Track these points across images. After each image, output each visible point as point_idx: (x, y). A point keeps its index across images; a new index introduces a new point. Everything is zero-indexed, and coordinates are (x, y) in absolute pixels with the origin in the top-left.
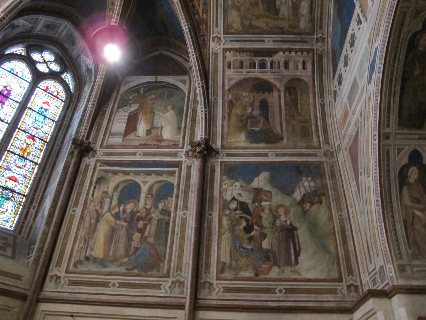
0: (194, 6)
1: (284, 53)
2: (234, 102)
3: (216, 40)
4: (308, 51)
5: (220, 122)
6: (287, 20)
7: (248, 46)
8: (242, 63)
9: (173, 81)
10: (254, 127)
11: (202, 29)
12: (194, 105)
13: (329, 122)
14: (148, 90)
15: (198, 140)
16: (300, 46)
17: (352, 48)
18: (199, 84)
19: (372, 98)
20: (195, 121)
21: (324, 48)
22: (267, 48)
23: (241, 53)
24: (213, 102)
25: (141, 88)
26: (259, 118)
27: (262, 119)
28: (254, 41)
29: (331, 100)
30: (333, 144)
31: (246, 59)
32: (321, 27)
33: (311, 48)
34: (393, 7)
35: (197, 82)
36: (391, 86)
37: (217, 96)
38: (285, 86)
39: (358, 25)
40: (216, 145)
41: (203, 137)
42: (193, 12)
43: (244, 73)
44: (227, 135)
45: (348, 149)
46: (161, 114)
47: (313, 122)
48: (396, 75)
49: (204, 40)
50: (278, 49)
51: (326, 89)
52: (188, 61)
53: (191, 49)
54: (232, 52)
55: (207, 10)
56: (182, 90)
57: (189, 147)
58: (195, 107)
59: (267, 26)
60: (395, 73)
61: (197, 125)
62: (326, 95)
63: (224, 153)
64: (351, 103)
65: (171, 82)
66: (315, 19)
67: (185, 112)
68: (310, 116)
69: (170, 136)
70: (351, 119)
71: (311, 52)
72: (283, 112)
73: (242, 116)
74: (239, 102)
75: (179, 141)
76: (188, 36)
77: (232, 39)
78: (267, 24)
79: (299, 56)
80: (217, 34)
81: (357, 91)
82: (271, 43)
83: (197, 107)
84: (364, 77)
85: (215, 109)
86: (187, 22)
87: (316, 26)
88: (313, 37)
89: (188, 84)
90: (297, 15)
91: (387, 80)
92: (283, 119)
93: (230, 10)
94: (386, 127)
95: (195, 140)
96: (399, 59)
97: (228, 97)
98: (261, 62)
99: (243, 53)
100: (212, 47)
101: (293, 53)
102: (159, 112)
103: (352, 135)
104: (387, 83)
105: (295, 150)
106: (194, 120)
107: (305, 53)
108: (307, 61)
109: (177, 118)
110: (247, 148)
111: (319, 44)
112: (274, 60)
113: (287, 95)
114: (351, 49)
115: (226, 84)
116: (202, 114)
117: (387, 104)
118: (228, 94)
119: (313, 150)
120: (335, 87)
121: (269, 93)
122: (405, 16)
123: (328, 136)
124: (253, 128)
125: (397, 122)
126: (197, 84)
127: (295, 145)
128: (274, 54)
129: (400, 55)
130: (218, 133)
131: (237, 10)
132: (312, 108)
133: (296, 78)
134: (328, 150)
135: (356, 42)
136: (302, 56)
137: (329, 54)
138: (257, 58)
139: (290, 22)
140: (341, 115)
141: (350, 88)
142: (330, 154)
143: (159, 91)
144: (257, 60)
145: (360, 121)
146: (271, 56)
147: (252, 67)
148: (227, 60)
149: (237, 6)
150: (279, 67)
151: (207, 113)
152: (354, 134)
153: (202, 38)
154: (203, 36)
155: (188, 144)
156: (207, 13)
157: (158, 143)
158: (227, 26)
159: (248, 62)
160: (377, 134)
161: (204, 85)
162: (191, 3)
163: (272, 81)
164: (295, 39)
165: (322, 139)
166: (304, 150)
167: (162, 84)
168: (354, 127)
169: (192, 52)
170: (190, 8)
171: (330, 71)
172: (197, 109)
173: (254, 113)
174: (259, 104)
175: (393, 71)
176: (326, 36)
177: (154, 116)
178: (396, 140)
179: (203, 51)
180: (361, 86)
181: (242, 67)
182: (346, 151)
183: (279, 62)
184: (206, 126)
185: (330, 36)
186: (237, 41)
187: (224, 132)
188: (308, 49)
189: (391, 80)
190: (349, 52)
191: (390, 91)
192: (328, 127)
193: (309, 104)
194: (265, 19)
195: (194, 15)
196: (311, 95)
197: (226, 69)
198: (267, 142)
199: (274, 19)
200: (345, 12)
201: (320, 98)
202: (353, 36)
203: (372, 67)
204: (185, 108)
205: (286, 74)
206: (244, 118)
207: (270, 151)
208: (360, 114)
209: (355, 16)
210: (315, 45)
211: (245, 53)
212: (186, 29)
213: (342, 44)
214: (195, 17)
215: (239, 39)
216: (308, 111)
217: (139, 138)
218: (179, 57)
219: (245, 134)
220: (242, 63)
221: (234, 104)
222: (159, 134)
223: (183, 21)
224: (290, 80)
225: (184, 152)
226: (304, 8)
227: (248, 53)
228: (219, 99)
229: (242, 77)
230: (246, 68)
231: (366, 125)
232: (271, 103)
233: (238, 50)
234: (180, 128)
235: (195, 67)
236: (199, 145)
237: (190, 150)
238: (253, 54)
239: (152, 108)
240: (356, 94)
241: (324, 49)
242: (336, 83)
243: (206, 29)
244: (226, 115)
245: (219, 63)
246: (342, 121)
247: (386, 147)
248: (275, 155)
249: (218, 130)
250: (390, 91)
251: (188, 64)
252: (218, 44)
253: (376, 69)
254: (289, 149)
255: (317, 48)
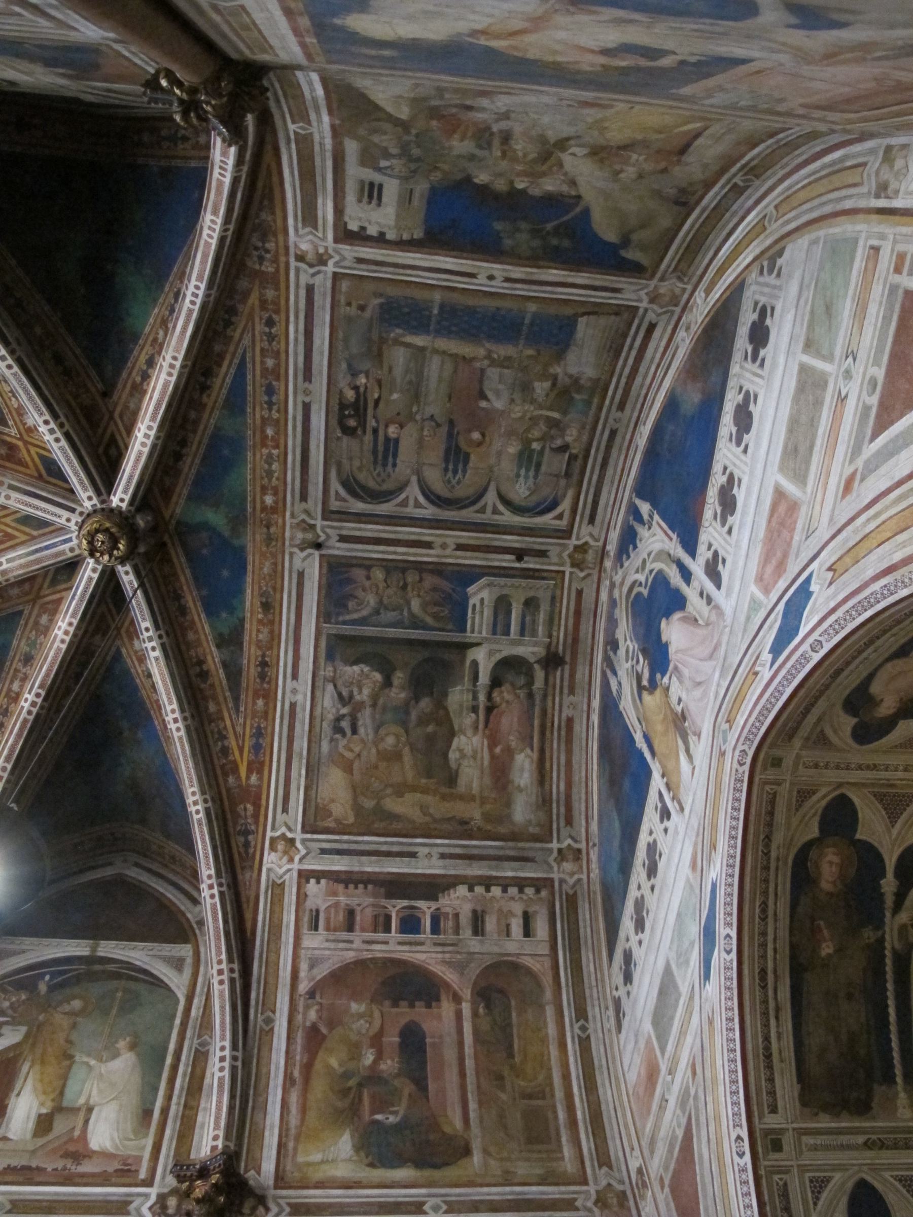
0: (225, 751)
1: (471, 889)
2: (324, 1030)
3: (281, 846)
4: (539, 884)
5: (276, 1095)
6: (478, 801)
7: (370, 866)
8: (351, 913)
9: (146, 959)
10: (378, 1113)
11: (243, 813)
12: (199, 1036)
13: (606, 1093)
14: (61, 985)
15: (203, 1154)
16: (513, 870)
17: (652, 880)
18: (220, 972)
19: (717, 1024)
20: (200, 1089)
21: (581, 876)
22: (424, 875)
23: (351, 886)
24: (262, 1030)
25: (42, 976)
26: (396, 1083)
27: (408, 1088)
28: (388, 854)
29: (606, 1026)
30: (623, 1168)
31: (365, 904)
32: (569, 821)
33: (545, 876)
34: (742, 781)
35: (216, 967)
36: (764, 987)
37: (274, 1012)
38: (475, 983)
39: (662, 821)
40: (259, 1173)
41: (220, 1146)
42: (222, 767)
43: (357, 944)
44: (297, 1139)
45: (667, 1182)
46: (93, 1062)
47: (559, 1094)
48: (775, 959)
49: (247, 844)
50: (456, 876)
51: (592, 993)
52: (195, 902)
53: (207, 870)
54: (323, 881)
55: (262, 764)
56: (169, 989)
57: (171, 1181)
58: (203, 1044)
59: (425, 815)
60: (770, 953)
61: (202, 1105)
62: (593, 1011)
63: (282, 1202)
64: (662, 1037)
65: (138, 963)
66: (551, 799)
67: (169, 1060)
68: (550, 1077)
69: (112, 1139)
70: (668, 1087)
71: (545, 886)
72: (469, 1063)
73: (346, 1076)
74: (339, 1031)
75: (139, 1159)
76: (201, 832)
77: (325, 845)
78: (424, 809)
79: (512, 898)
80: (284, 829)
81: (677, 1001)
82: (435, 861)
83: (209, 1044)
84: (692, 963)
85: (264, 1053)
86: (203, 793)
87: (555, 817)
88: (549, 846)
89: (188, 971)
90: (504, 787)
91: (752, 971)
92: (469, 1088)
93: (323, 768)
94: (766, 1111)
95: (192, 1156)
96: (775, 914)
97: (305, 1014)
98: (408, 912)
99: (356, 888)
100: (270, 866)
101: (496, 891)
102: (89, 1055)
103: (674, 1137)
104: (754, 977)
105: (508, 1189)
106: (196, 1087)
107: (530, 891)
108: (536, 912)
109: (143, 1078)
110: (358, 1185)
111: (568, 866)
112: (443, 910)
113: (481, 1010)
114: (649, 884)
115: (303, 974)
116: (222, 1069)
117: (760, 1040)
118: (307, 1007)
119: (563, 1188)
120: (617, 989)
121: (429, 1006)
122: (772, 802)
123: (605, 1138)
124: (379, 1117)
125: (796, 1094)
126: (215, 972)
127: (507, 1172)
128: (443, 892)
129: (776, 904)
130: (267, 1134)
131: (345, 771)
132: (554, 1052)
133: (505, 962)
134: (609, 1185)
135: (661, 865)
136: (521, 898)
137: (595, 893)
138: (394, 901)
139: (488, 807)
140: (639, 1073)
141: (655, 993)
142: (615, 1201)
143: (96, 989)
144: (396, 907)
145: (692, 1092)
146: (432, 896)
147: (381, 929)
148: (310, 904)
149: (343, 756)
150: (457, 930)
151: (239, 1064)
152: (680, 1133)
153: (242, 839)
154: (246, 833)
155: (169, 1168)
156: (260, 772)
157: (69, 1164)
158: (313, 808)
159: (369, 912)
160: (745, 1134)
161: (236, 975)
162: (220, 744)
163: (438, 969)
164: (501, 853)
165: (590, 1149)
166: (534, 1188)
167: (111, 967)
168: (678, 1112)
169: (210, 877)
170: (215, 757)
171: (599, 939)
172: (208, 1051)
173: (383, 1067)
174: (397, 1039)
175: (764, 945)
176: (583, 846)
177: (70, 1067)
178: (801, 1152)
179: (240, 877)
180: (684, 989)
181: (350, 927)
182: (662, 1188)
183: (457, 915)
184: (231, 1108)
185: (594, 845)
186: (339, 852)
187: (288, 1130)
188: (538, 879)
189: (763, 972)
190: (646, 886)
191: (765, 1002)
192: (603, 1107)
193: (544, 1040)
194: (419, 795)
195: (226, 775)
196: (550, 1011)
197: (305, 930)
198: (419, 1164)
199: (444, 798)
200: (627, 784)
201: (577, 1021)
202: (652, 848)
203: (709, 934)
204: (172, 1046)
205: (476, 950)
206: (352, 1083)
207: (430, 1196)
208: (689, 1073)
209: (652, 799)
210: (556, 869)
211: (361, 886)
212: (197, 812)
213: (626, 868)
214: (226, 781)
215: (345, 846)
216: (543, 1063)
217: (8, 1146)
218: (170, 888)
219: (352, 1136)
220: (351, 913)
221: (324, 1037)
222: (77, 1133)
223: (192, 789)
224: (487, 968)
225: (153, 1198)
226: (522, 770)
227: (370, 887)
228: (277, 1023)
229: (350, 956)
230: (363, 930)
231: (710, 1107)
232: (433, 1037)
233: (343, 877)
234: (147, 1114)
235: (215, 919)
236: (203, 1172)
237: (174, 1192)
238: (382, 890)
239: (69, 1042)
240: (675, 1010)
241: (579, 880)
242: (619, 979)
243: (256, 816)
244: (296, 1074)
245: (285, 913)
246: (641, 1091)
247: (776, 1178)
248: (445, 1207)
249: (268, 1122)
250: (765, 1002)
251: (197, 909)
252: (285, 859)
253: (720, 942)
254: (488, 1185)
255: (562, 876)
